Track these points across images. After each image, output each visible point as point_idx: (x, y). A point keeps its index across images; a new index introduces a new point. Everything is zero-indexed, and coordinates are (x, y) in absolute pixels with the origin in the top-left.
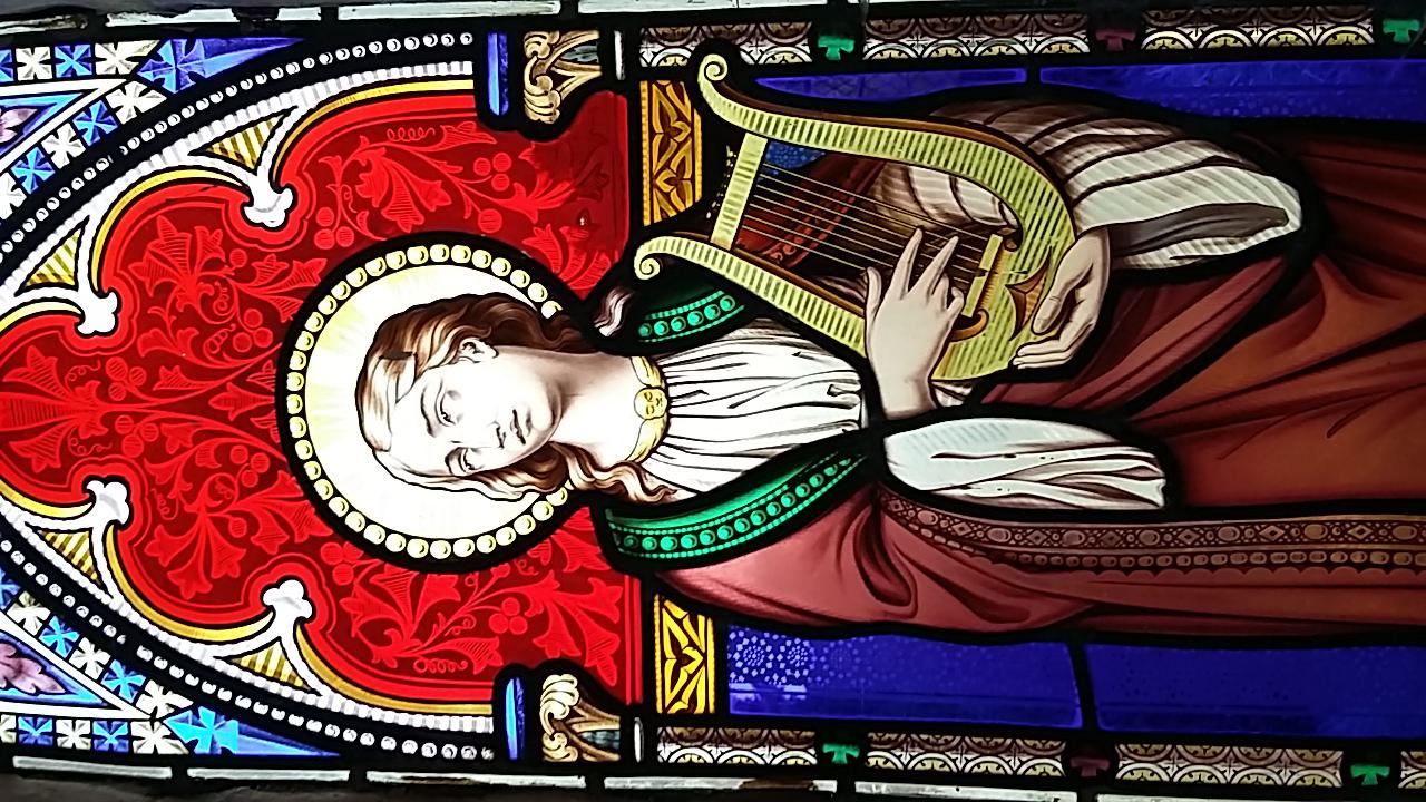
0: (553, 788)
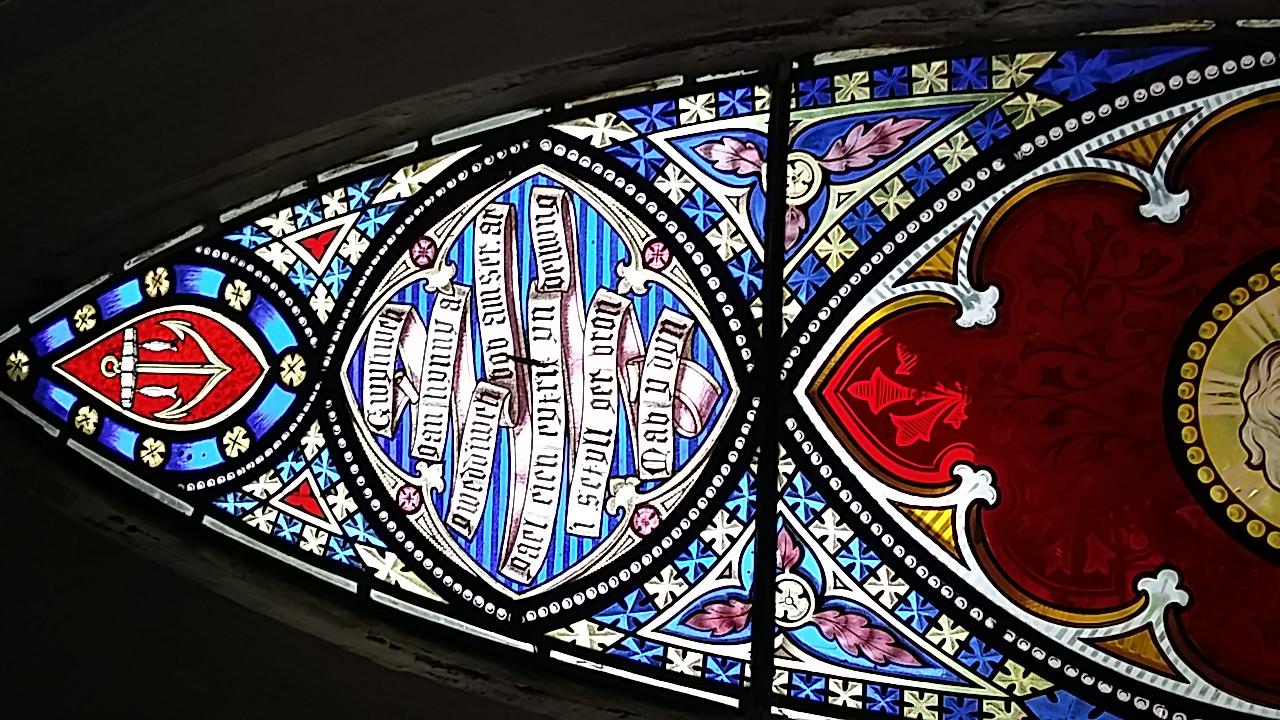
0: (176, 237)
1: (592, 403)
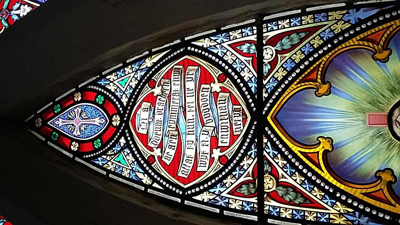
1: (206, 163)
